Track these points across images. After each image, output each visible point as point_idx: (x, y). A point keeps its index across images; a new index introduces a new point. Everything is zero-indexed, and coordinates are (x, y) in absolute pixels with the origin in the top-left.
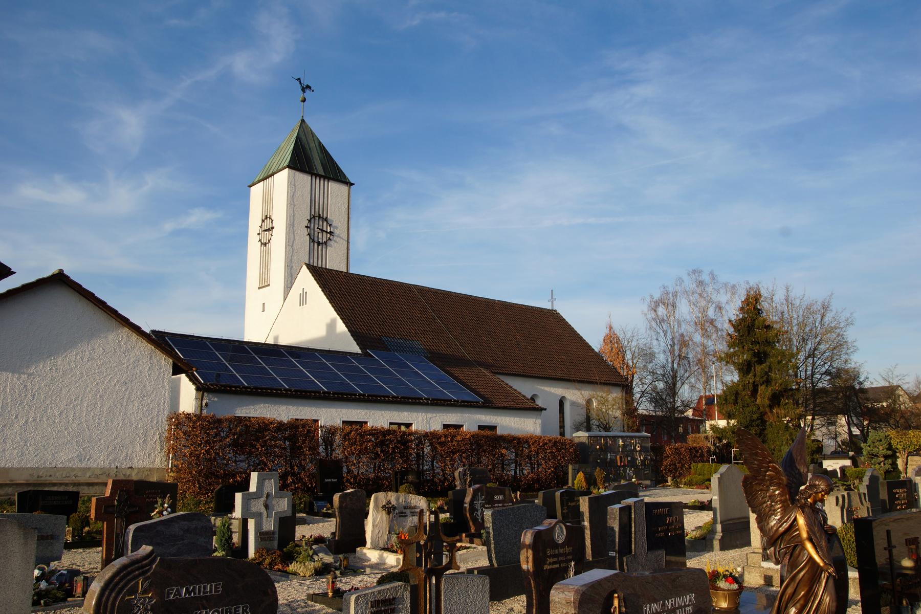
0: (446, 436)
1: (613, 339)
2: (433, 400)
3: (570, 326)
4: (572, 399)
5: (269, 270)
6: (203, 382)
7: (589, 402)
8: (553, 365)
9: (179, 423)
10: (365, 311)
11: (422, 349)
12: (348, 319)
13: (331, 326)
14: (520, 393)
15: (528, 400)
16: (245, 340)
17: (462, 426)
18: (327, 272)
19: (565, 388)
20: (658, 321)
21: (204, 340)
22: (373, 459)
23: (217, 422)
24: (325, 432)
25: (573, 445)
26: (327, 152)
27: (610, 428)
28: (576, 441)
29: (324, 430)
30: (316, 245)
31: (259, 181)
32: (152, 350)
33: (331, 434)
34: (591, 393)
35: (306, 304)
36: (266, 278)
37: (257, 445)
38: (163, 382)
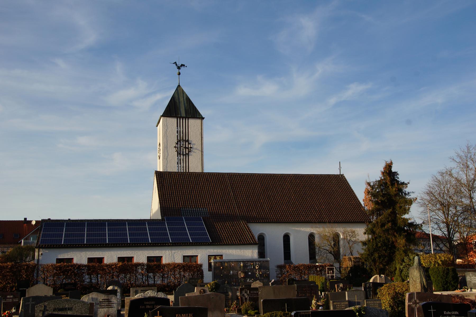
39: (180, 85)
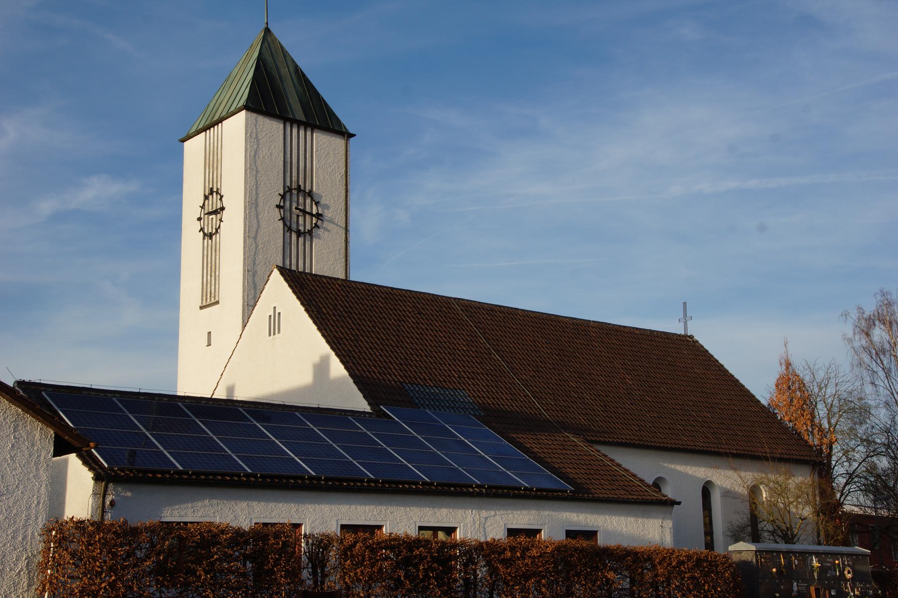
0: (513, 549)
1: (793, 383)
2: (490, 487)
3: (717, 361)
4: (725, 486)
5: (217, 278)
6: (106, 466)
7: (754, 490)
8: (690, 428)
9: (64, 538)
10: (376, 343)
11: (471, 403)
12: (348, 356)
13: (321, 368)
14: (634, 476)
15: (648, 486)
16: (179, 394)
17: (539, 531)
18: (313, 280)
19: (711, 467)
20: (874, 352)
21: (109, 395)
22: (393, 590)
23: (130, 533)
24: (312, 544)
25: (730, 565)
26: (310, 82)
27: (794, 536)
28: (735, 558)
29: (310, 541)
30: (294, 236)
31: (198, 132)
32: (18, 415)
33: (322, 547)
34: (758, 475)
35: (279, 332)
36: (213, 291)
37: (197, 570)
38: (37, 469)
39: (269, 27)
